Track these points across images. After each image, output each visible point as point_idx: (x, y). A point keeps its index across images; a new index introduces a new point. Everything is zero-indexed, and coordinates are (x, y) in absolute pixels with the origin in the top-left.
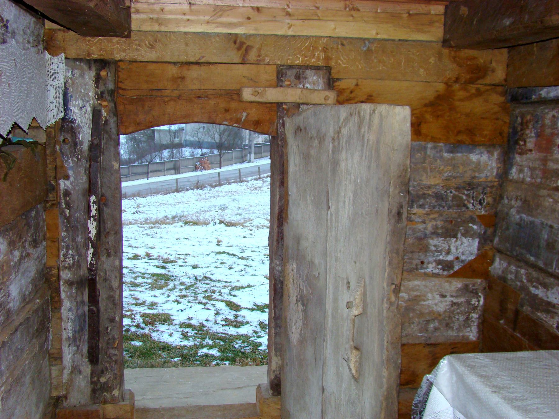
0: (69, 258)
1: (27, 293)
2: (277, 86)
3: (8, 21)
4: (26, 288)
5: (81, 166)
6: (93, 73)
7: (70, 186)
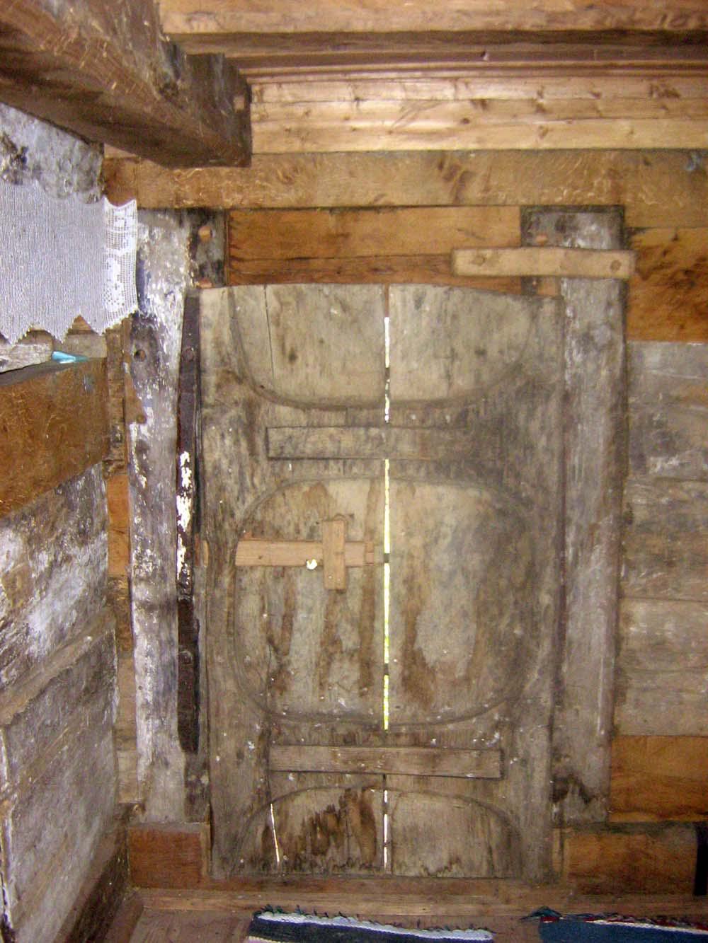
0: (146, 562)
1: (67, 625)
2: (522, 246)
3: (24, 149)
4: (65, 619)
5: (165, 400)
6: (185, 233)
7: (147, 434)
